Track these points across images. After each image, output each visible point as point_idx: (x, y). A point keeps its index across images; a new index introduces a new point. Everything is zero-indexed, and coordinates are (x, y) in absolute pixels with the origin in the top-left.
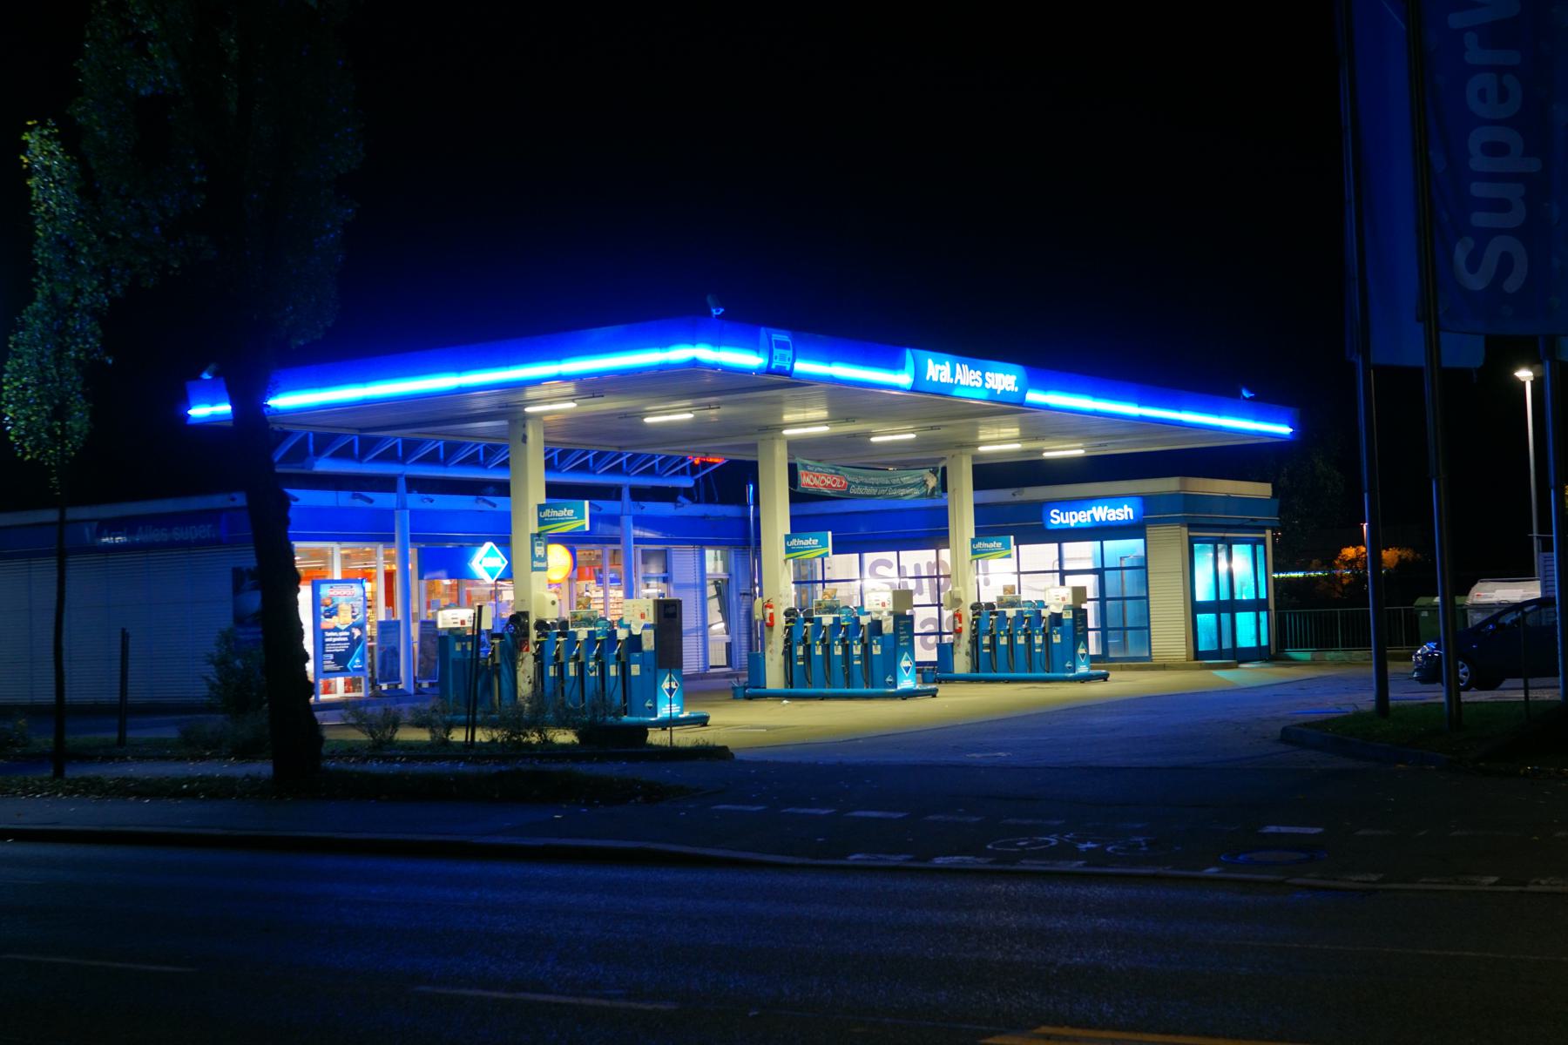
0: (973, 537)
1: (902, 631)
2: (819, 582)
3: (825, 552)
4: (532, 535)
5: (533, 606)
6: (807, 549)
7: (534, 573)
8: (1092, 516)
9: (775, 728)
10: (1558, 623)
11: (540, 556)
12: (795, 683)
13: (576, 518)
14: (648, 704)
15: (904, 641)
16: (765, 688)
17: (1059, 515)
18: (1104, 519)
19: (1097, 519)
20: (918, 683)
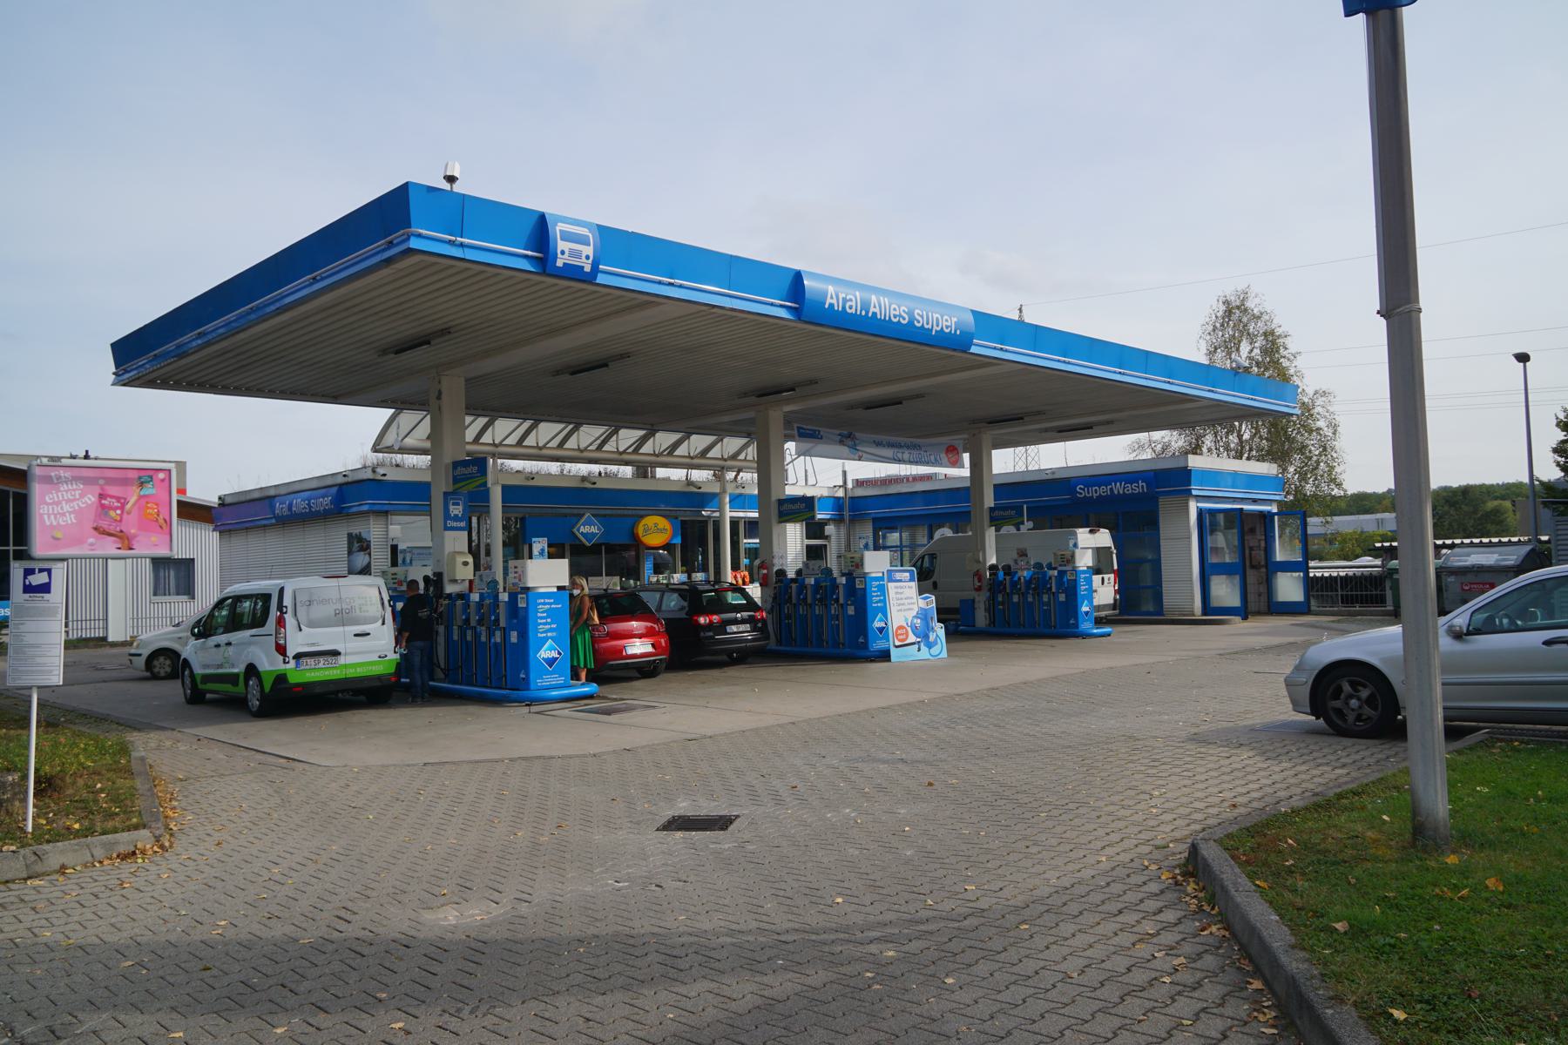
0: (114, 370)
1: (874, 592)
2: (905, 546)
3: (483, 481)
4: (445, 493)
5: (446, 567)
6: (468, 479)
7: (447, 533)
8: (1111, 489)
9: (733, 685)
10: (728, 506)
11: (456, 516)
12: (996, 624)
13: (479, 475)
14: (1071, 622)
15: (877, 602)
16: (974, 626)
17: (1084, 490)
18: (1121, 492)
19: (1116, 492)
20: (132, 742)
